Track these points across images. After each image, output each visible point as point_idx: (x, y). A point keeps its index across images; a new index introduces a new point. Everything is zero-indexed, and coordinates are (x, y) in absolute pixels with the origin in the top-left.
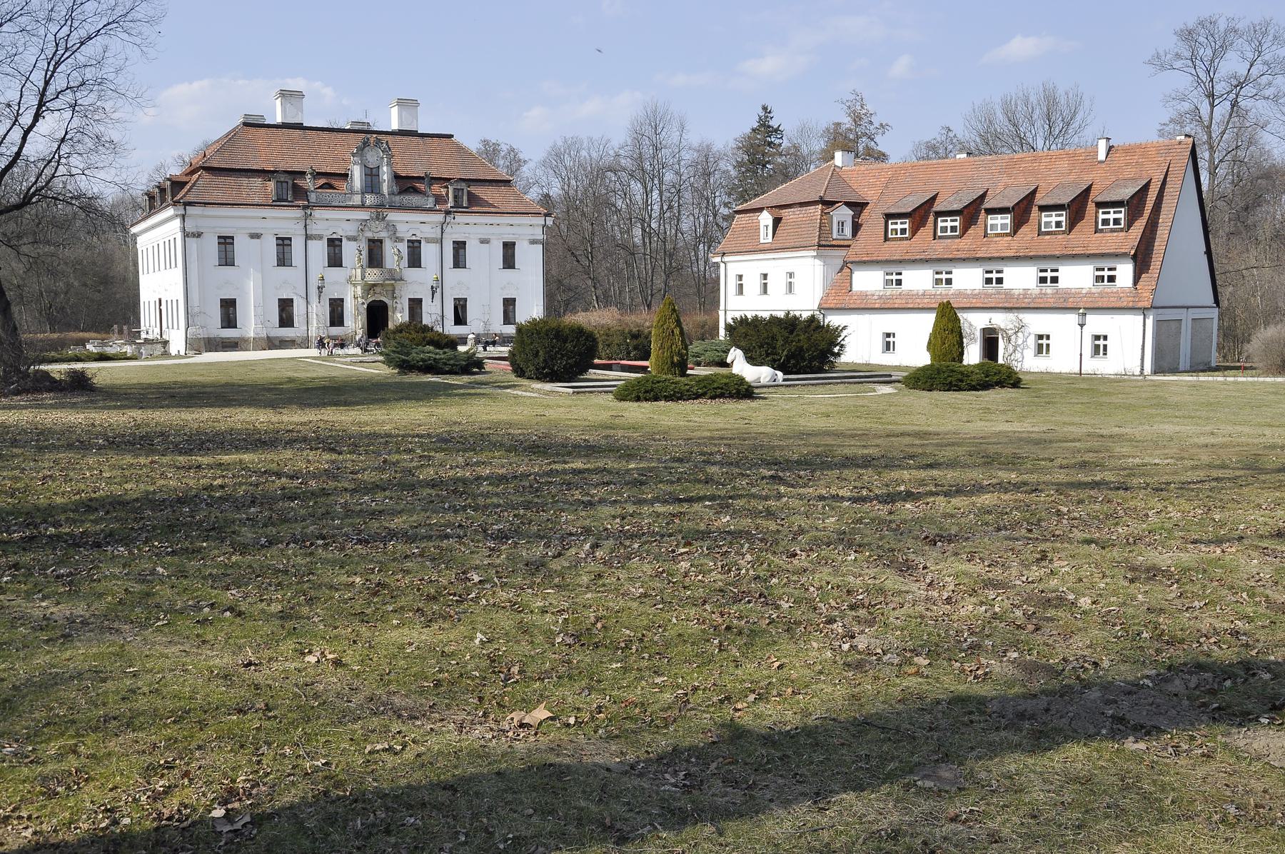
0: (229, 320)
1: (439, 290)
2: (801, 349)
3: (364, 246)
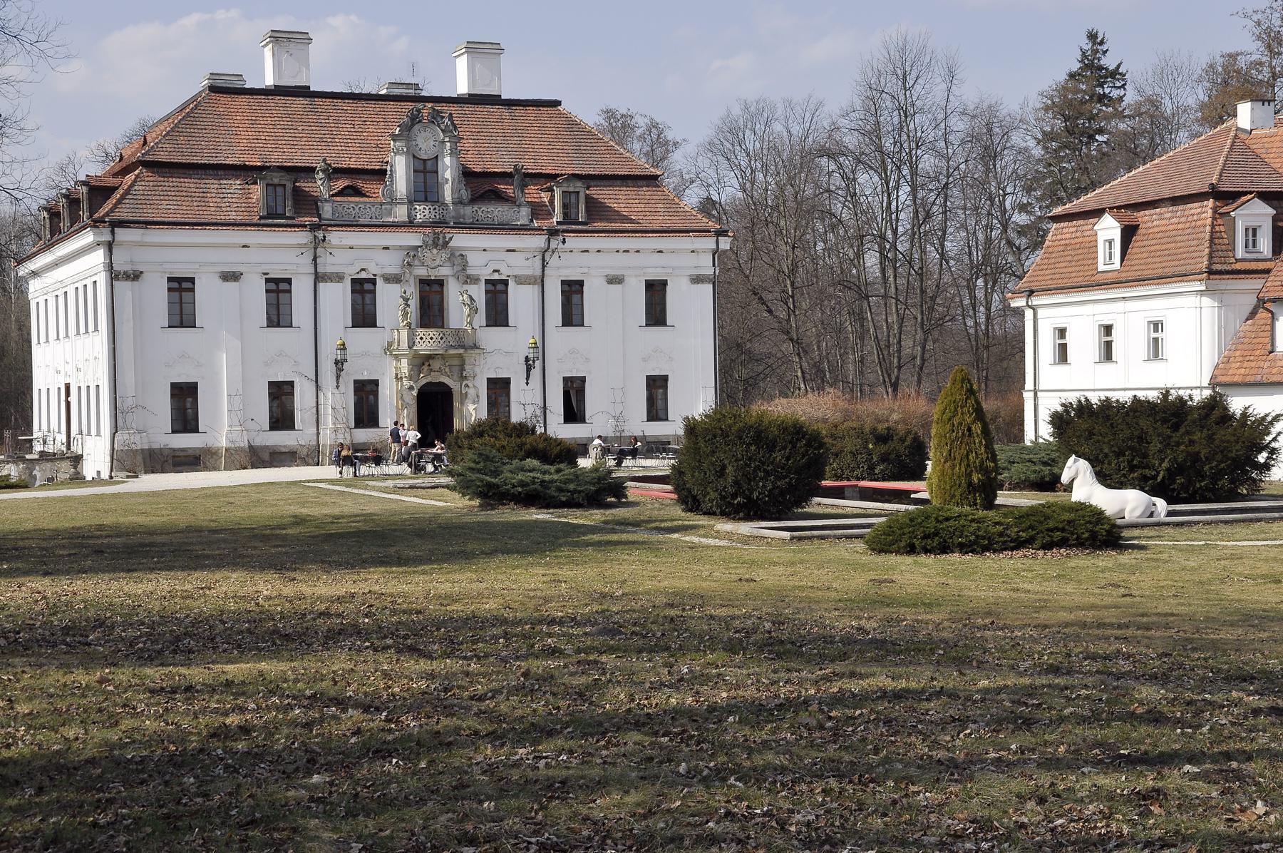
0: (185, 419)
1: (538, 364)
2: (1195, 457)
3: (412, 290)
